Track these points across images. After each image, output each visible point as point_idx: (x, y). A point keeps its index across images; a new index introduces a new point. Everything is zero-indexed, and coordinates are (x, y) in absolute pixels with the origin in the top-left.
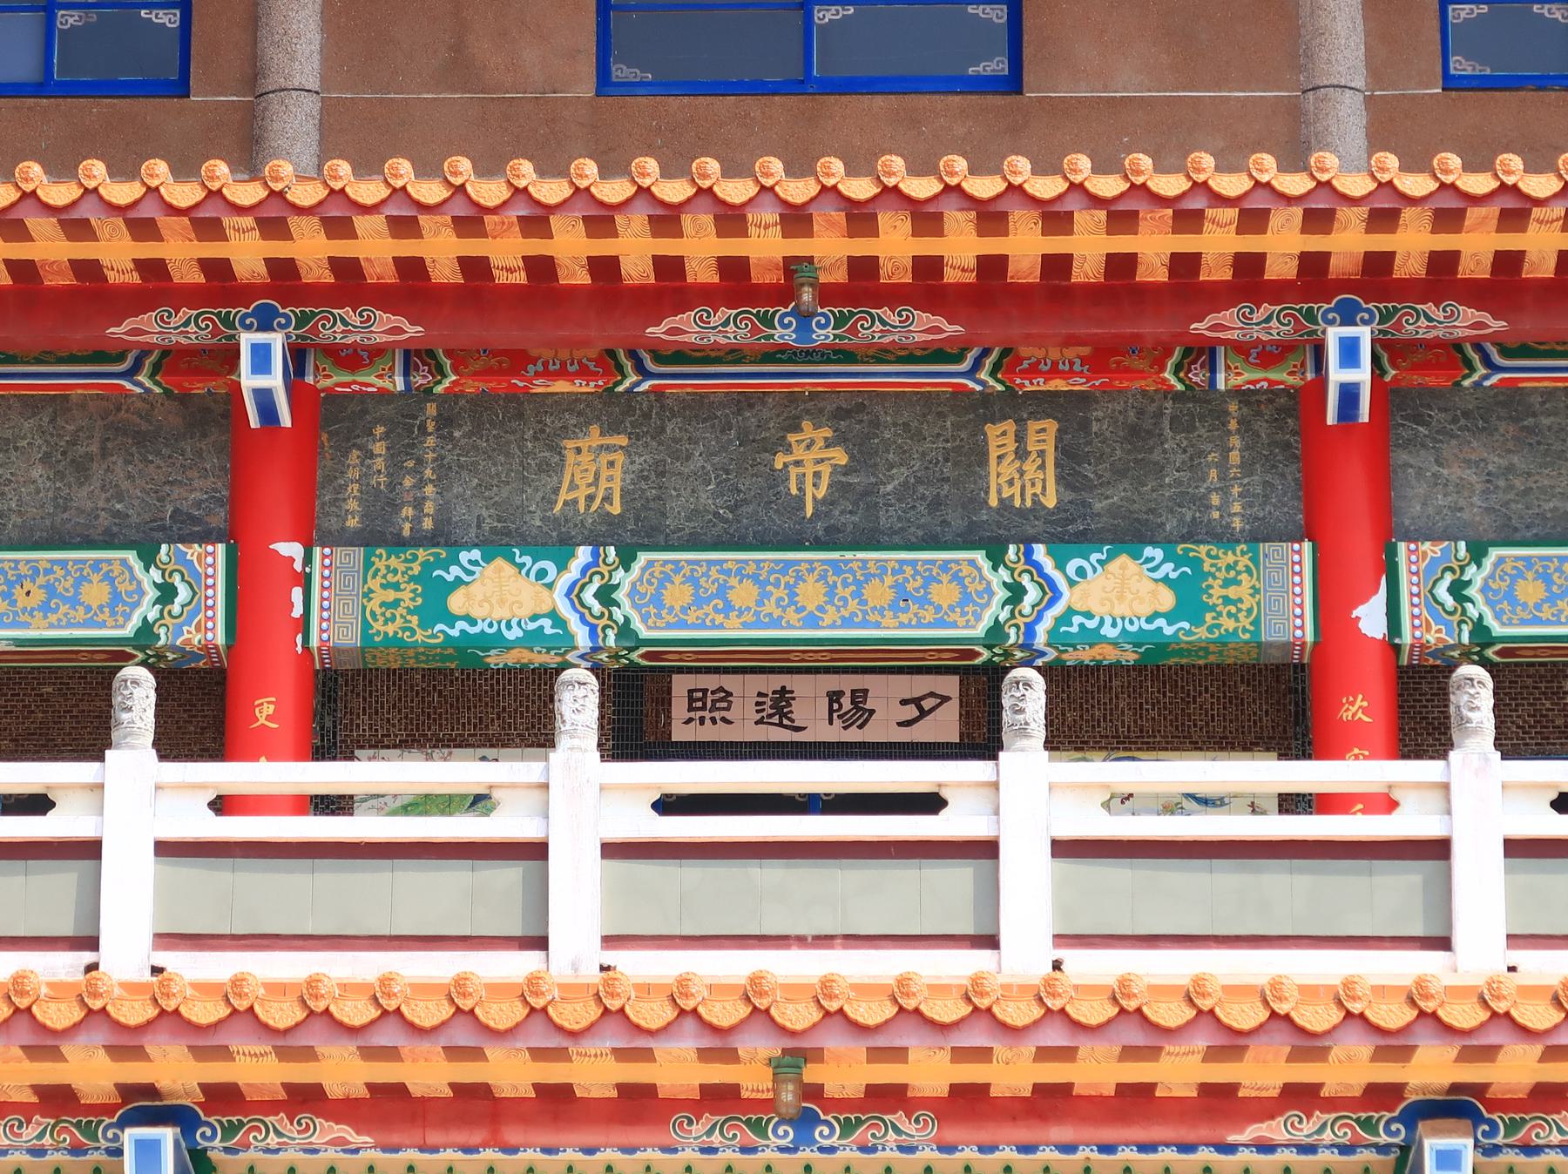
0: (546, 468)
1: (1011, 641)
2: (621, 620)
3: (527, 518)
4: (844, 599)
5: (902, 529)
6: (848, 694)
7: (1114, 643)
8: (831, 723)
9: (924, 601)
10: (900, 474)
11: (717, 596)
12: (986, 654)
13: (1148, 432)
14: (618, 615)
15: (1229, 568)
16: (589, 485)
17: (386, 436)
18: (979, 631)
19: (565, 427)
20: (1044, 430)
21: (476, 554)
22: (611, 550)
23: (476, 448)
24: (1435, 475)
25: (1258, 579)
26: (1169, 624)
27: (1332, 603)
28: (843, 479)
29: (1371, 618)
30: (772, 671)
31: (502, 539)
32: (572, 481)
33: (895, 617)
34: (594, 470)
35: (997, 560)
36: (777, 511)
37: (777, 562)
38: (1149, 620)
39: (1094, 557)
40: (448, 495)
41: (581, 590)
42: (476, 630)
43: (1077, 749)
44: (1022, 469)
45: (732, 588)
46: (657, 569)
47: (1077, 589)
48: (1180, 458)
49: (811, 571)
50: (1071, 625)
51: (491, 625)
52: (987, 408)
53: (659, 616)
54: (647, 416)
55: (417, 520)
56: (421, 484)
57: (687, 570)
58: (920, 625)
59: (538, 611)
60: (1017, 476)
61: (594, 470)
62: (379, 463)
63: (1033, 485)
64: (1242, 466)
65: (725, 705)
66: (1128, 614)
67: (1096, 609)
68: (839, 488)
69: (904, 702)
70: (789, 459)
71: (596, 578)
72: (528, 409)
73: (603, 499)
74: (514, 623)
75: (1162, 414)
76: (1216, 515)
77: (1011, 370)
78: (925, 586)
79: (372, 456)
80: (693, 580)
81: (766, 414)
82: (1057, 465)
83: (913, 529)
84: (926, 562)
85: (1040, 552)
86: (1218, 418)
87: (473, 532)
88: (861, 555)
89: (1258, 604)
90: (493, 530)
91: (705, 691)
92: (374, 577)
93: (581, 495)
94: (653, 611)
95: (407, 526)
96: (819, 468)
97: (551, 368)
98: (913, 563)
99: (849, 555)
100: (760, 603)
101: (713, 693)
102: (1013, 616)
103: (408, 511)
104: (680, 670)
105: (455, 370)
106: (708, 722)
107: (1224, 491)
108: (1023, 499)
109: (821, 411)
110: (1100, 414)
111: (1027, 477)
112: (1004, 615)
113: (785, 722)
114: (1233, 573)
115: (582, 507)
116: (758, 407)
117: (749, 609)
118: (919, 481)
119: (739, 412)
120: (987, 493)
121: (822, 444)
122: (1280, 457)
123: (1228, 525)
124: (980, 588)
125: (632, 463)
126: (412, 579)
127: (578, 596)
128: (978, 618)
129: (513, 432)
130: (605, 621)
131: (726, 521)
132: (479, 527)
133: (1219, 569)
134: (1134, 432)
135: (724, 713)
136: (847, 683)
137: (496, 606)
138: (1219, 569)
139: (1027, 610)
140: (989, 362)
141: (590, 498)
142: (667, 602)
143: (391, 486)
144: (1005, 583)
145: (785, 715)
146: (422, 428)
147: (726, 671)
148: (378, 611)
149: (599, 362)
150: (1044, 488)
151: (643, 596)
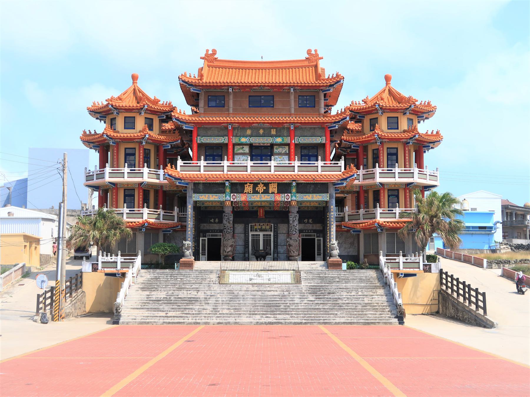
24: (298, 132)
27: (291, 141)
29: (293, 142)
31: (243, 136)
34: (249, 132)
44: (273, 132)
61: (249, 132)
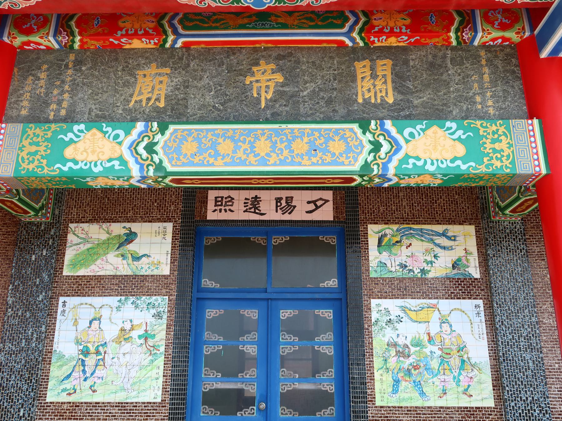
0: (127, 84)
1: (375, 173)
2: (157, 161)
3: (115, 109)
4: (281, 150)
5: (312, 114)
6: (284, 199)
7: (433, 175)
8: (277, 211)
9: (326, 151)
10: (311, 87)
11: (211, 148)
12: (359, 180)
13: (439, 65)
14: (156, 159)
15: (494, 133)
16: (149, 92)
17: (48, 70)
18: (357, 167)
19: (138, 65)
20: (385, 65)
21: (82, 126)
22: (155, 124)
23: (93, 75)
25: (511, 139)
26: (464, 163)
28: (281, 89)
30: (251, 189)
31: (101, 117)
32: (140, 91)
33: (310, 159)
35: (365, 128)
36: (246, 105)
37: (244, 130)
38: (452, 161)
39: (419, 127)
40: (75, 98)
41: (137, 145)
42: (78, 167)
43: (385, 224)
45: (220, 143)
46: (179, 133)
47: (410, 144)
48: (457, 78)
49: (263, 134)
50: (408, 164)
51: (86, 165)
52: (355, 54)
53: (178, 159)
54: (181, 59)
55: (58, 111)
56: (62, 93)
57: (195, 134)
58: (323, 164)
59: (113, 156)
60: (372, 87)
62: (42, 83)
63: (381, 91)
64: (491, 82)
65: (231, 203)
66: (440, 158)
67: (421, 155)
68: (279, 94)
69: (309, 202)
70: (253, 79)
71: (146, 139)
72: (121, 56)
73: (156, 100)
74: (99, 163)
75: (446, 57)
76: (479, 107)
77: (369, 32)
78: (326, 143)
79: (39, 79)
80: (198, 140)
81: (241, 57)
82: (393, 82)
83: (318, 114)
84: (326, 130)
85: (388, 124)
86: (475, 59)
87: (86, 116)
88: (290, 126)
89: (513, 152)
90: (97, 116)
91: (222, 198)
92: (26, 139)
93: (144, 97)
94: (175, 156)
95: (52, 113)
96: (268, 84)
97: (130, 32)
98: (319, 130)
99: (284, 126)
100: (234, 152)
101: (226, 198)
102: (375, 159)
103: (54, 106)
104: (212, 189)
105: (80, 34)
106: (223, 211)
107: (483, 94)
108: (376, 99)
109: (270, 56)
110: (414, 57)
111: (377, 88)
112: (370, 158)
113: (257, 211)
114: (496, 136)
115: (144, 104)
116: (238, 54)
117: (228, 155)
118: (321, 90)
119: (228, 57)
120: (357, 96)
121: (270, 72)
122: (510, 78)
123: (486, 112)
124: (356, 143)
125: (172, 81)
126: (47, 140)
127: (135, 149)
128: (356, 160)
129: (112, 67)
130: (148, 162)
131: (219, 110)
132: (89, 114)
133: (489, 134)
134: (432, 65)
135: (230, 207)
136: (284, 194)
137: (90, 154)
138: (489, 134)
139: (383, 156)
140: (357, 28)
141: (149, 99)
142: (184, 151)
143: (47, 94)
144: (370, 141)
145: (257, 208)
146: (67, 66)
147: (232, 189)
148: (26, 157)
149: (155, 29)
150: (387, 93)
151: (170, 148)
